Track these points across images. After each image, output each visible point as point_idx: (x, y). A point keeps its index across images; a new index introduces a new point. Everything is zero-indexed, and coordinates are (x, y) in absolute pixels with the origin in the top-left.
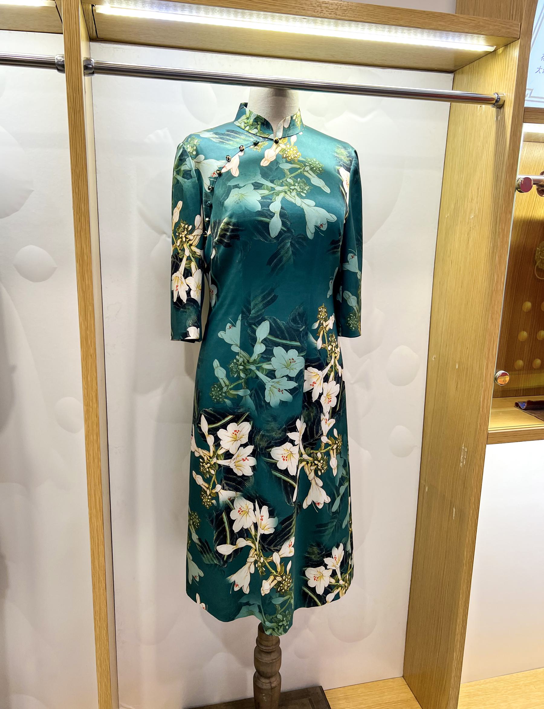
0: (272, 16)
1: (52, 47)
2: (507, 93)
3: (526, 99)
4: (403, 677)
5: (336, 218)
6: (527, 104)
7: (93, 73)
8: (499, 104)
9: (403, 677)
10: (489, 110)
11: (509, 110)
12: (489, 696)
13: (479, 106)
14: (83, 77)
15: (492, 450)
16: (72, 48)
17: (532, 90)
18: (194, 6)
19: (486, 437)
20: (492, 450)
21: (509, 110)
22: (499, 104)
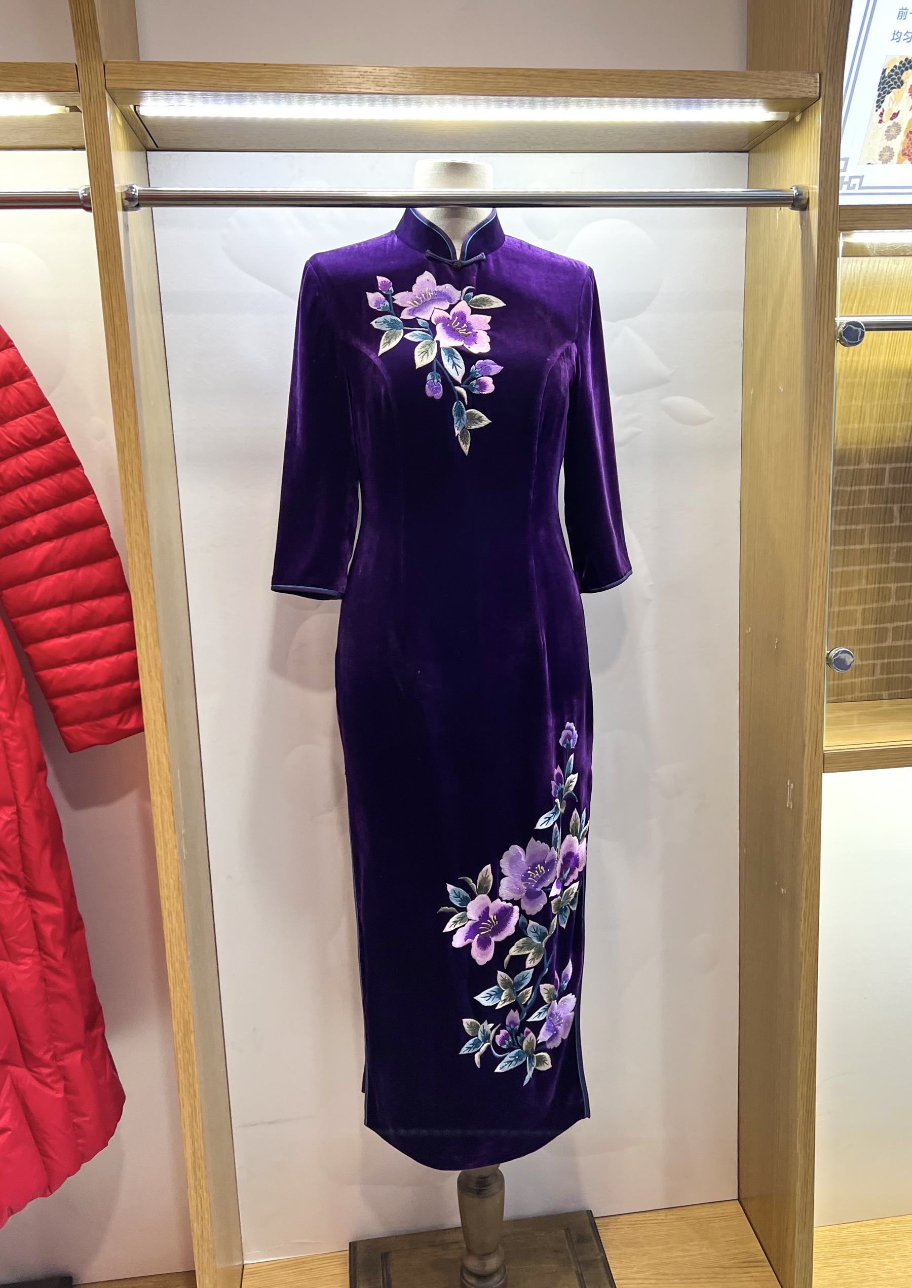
0: (665, 102)
1: (69, 172)
2: (813, 189)
3: (840, 192)
4: (738, 1199)
5: (439, 395)
6: (843, 201)
7: (138, 206)
8: (799, 203)
9: (738, 1199)
10: (791, 215)
11: (814, 212)
12: (899, 1243)
13: (778, 209)
14: (120, 213)
15: (831, 782)
16: (100, 169)
17: (861, 178)
18: (562, 99)
19: (822, 758)
20: (831, 782)
21: (814, 212)
22: (799, 203)
